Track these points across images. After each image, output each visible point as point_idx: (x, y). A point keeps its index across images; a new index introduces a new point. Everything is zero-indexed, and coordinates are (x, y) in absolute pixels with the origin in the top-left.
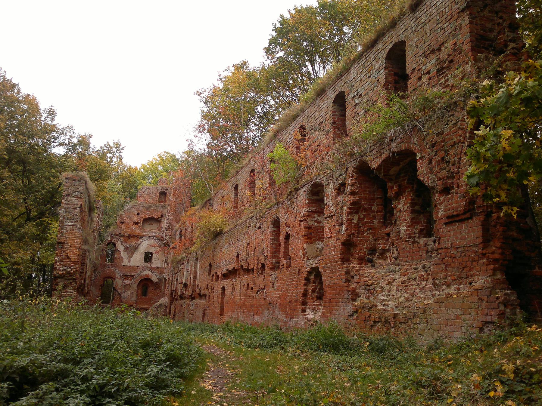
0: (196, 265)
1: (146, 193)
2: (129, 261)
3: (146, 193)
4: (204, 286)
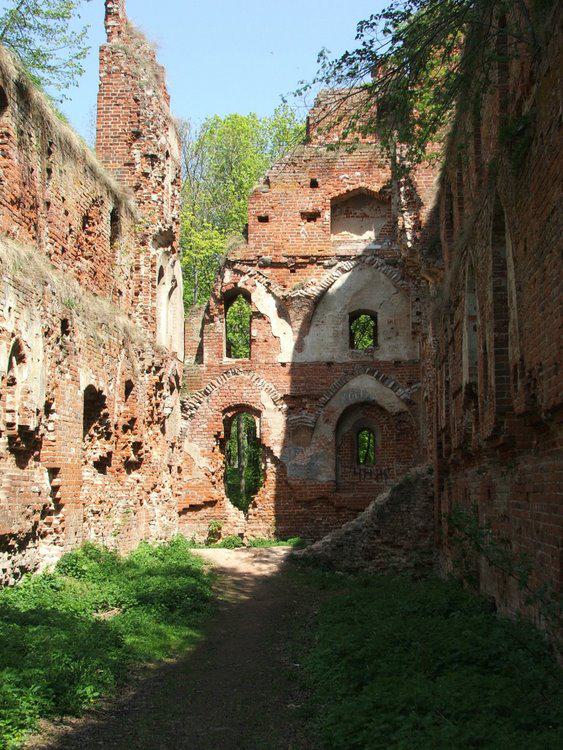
0: (500, 270)
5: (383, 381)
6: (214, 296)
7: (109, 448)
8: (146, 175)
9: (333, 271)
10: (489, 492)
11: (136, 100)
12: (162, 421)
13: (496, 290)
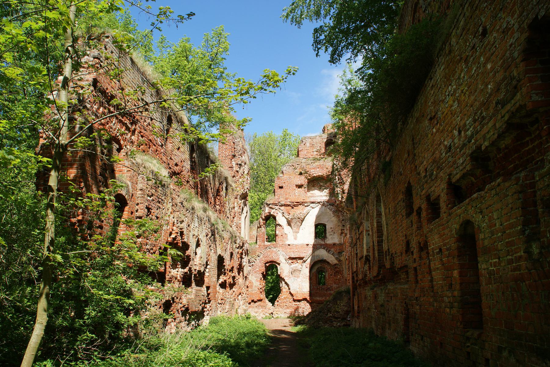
0: (379, 215)
1: (308, 144)
2: (295, 239)
3: (308, 144)
4: (398, 247)
6: (262, 218)
8: (237, 171)
9: (308, 208)
10: (376, 297)
11: (234, 143)
13: (378, 222)
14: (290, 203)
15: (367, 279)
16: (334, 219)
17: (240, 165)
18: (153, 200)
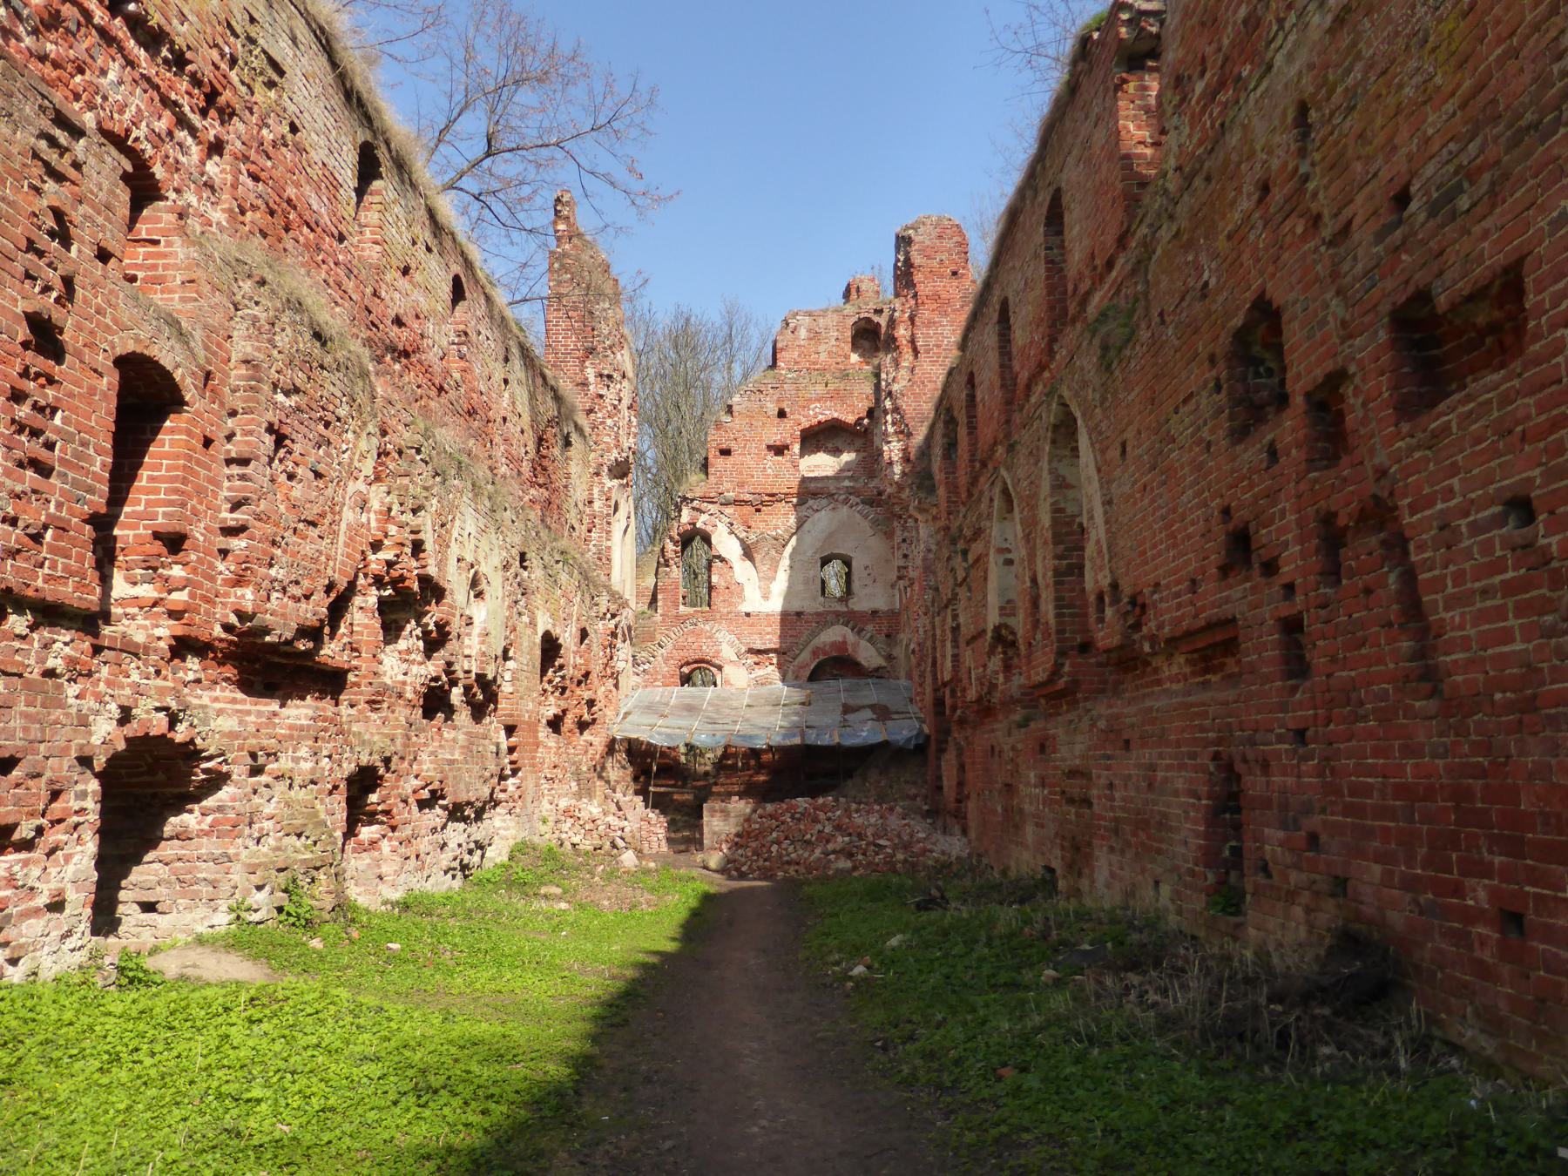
1: (803, 333)
3: (803, 333)
5: (859, 633)
6: (671, 538)
7: (563, 704)
12: (615, 676)
14: (748, 497)
15: (996, 698)
16: (877, 544)
17: (610, 377)
18: (298, 409)
